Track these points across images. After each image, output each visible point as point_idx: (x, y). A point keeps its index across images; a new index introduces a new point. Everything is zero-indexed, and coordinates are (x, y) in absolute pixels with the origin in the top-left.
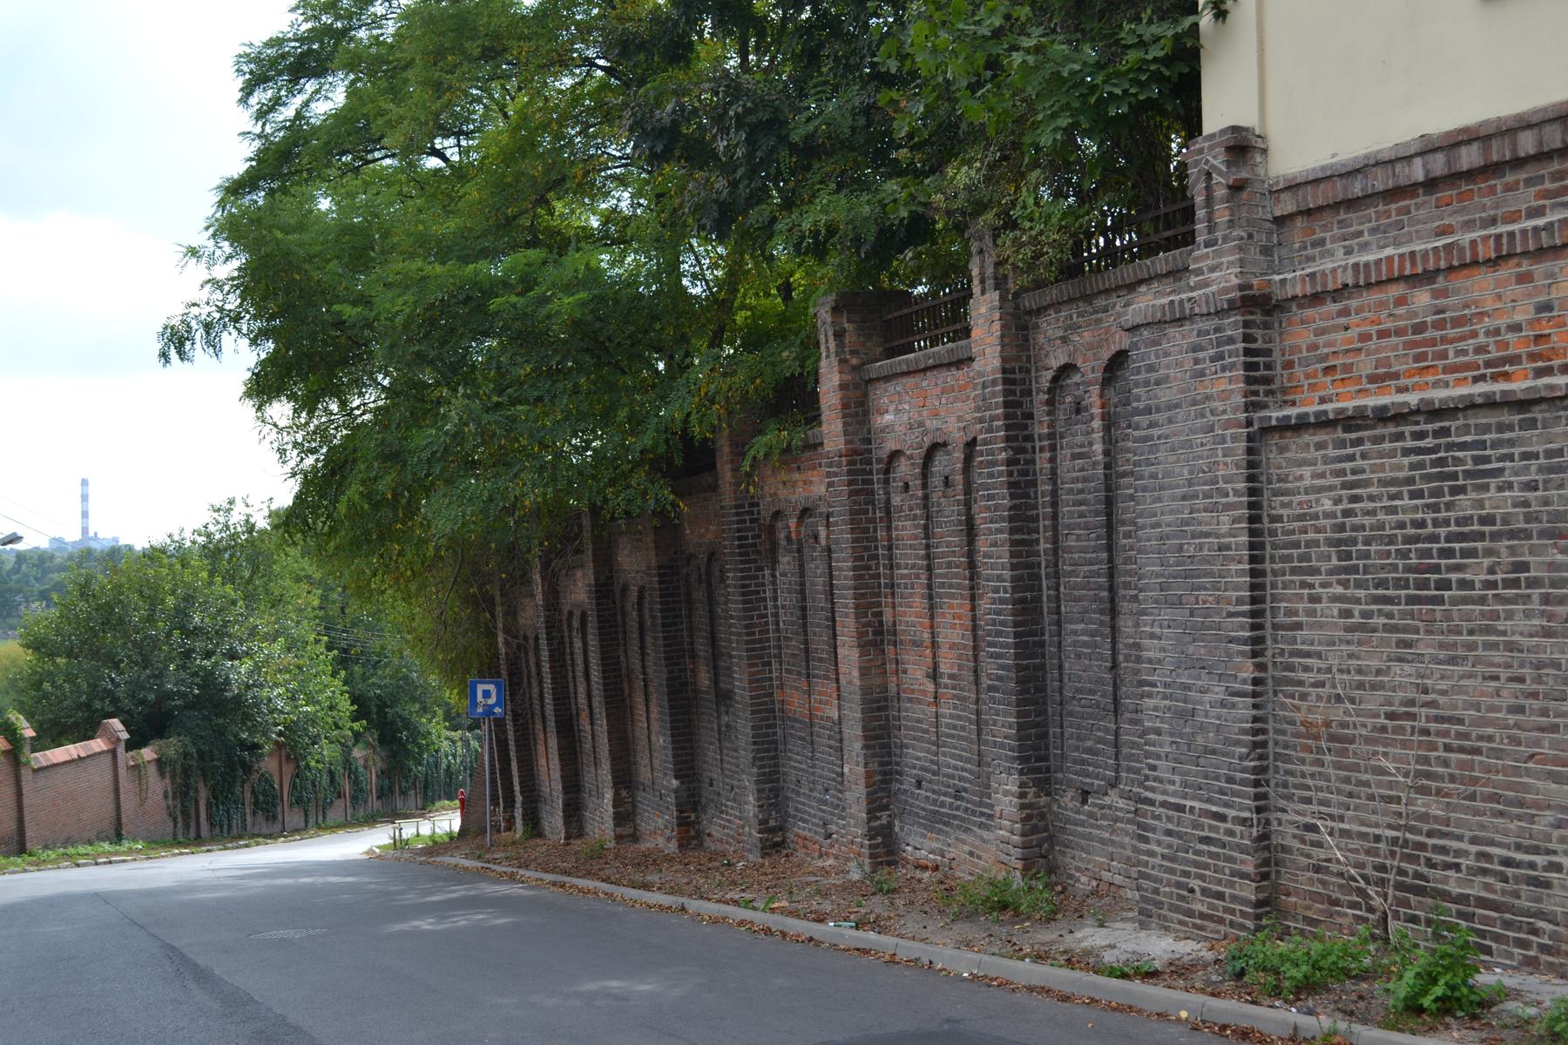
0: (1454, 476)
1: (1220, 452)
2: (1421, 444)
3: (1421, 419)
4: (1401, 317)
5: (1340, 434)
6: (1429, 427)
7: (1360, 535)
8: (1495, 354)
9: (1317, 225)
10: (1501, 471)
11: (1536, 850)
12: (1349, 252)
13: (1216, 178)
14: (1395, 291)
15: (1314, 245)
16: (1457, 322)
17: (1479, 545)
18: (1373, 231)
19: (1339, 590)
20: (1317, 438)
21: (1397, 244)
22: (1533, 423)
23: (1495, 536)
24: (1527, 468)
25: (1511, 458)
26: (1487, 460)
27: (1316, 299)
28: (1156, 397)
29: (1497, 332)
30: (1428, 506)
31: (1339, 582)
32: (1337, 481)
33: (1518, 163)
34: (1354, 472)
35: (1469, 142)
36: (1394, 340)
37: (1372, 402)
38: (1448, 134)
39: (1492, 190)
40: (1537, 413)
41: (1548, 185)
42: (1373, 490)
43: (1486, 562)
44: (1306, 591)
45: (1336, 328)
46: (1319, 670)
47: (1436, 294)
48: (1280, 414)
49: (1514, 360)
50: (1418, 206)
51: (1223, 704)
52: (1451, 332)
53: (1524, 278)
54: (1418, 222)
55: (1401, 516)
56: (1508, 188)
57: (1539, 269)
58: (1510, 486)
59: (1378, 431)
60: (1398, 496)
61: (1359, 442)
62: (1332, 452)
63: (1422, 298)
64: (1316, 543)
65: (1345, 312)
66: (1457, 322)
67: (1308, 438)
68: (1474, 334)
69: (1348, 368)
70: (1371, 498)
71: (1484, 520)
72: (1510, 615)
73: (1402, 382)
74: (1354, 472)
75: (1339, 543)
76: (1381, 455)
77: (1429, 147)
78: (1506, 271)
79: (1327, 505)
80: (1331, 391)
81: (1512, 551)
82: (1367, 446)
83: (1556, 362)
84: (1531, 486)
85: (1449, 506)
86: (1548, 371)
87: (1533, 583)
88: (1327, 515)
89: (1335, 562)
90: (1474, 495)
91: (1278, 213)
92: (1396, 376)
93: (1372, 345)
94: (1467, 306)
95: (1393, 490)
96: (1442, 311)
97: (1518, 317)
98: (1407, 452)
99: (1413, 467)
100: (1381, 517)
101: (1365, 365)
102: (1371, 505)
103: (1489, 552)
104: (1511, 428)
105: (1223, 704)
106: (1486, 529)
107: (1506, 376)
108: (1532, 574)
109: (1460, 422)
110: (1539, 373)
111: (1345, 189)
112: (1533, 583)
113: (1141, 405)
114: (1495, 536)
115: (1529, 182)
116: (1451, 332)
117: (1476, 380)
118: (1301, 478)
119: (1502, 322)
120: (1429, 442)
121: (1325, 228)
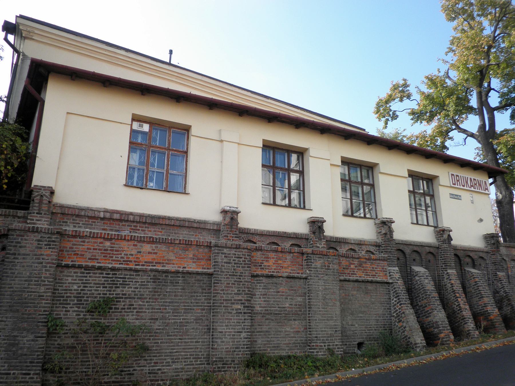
0: (117, 284)
1: (44, 270)
2: (108, 276)
3: (109, 270)
4: (101, 246)
5: (83, 270)
6: (111, 273)
7: (86, 296)
8: (125, 259)
9: (65, 218)
10: (129, 284)
11: (129, 367)
12: (75, 227)
13: (44, 198)
14: (99, 240)
15: (63, 222)
16: (116, 251)
17: (121, 300)
18: (83, 224)
19: (76, 309)
20: (75, 271)
21: (90, 228)
22: (139, 275)
23: (125, 298)
24: (136, 284)
25: (132, 282)
26: (126, 281)
27: (75, 237)
28: (19, 251)
29: (127, 255)
30: (108, 290)
31: (76, 307)
32: (81, 282)
33: (127, 221)
34: (86, 280)
35: (116, 213)
36: (98, 251)
37: (90, 264)
38: (112, 210)
39: (119, 225)
40: (140, 273)
41: (132, 227)
42: (92, 285)
43: (123, 304)
44: (64, 309)
45: (80, 245)
46: (66, 330)
47: (111, 244)
48: (66, 263)
49: (131, 261)
50: (98, 222)
51: (33, 340)
52: (115, 253)
53: (134, 245)
54: (97, 226)
55: (99, 292)
56: (123, 225)
57: (139, 244)
58: (131, 288)
59: (96, 272)
60: (99, 287)
61: (89, 273)
62: (79, 275)
63: (108, 244)
64: (70, 297)
65: (84, 242)
66: (116, 251)
67: (72, 270)
68: (121, 254)
69: (83, 255)
70: (90, 287)
71: (123, 294)
72: (128, 315)
73: (99, 261)
74: (86, 280)
75: (78, 297)
76: (96, 277)
77: (106, 211)
78: (132, 243)
79: (75, 287)
80: (75, 259)
81: (130, 301)
82: (91, 275)
83: (141, 264)
84: (137, 288)
85: (114, 291)
86: (139, 265)
87: (134, 309)
88: (75, 290)
89: (76, 302)
90: (121, 289)
91: (54, 211)
92: (97, 259)
93: (91, 251)
94: (119, 248)
95: (98, 286)
96: (113, 247)
97: (132, 253)
98: (103, 277)
99: (105, 281)
100: (93, 292)
101: (88, 255)
102: (90, 289)
103: (123, 301)
104: (133, 275)
105: (33, 340)
106: (124, 296)
107: (128, 264)
108: (134, 306)
109: (120, 273)
110: (136, 265)
111: (79, 212)
112: (134, 309)
113: (11, 252)
114: (125, 298)
115: (128, 226)
116: (115, 253)
117: (120, 264)
118: (67, 280)
119: (129, 253)
120: (111, 276)
121: (68, 219)
